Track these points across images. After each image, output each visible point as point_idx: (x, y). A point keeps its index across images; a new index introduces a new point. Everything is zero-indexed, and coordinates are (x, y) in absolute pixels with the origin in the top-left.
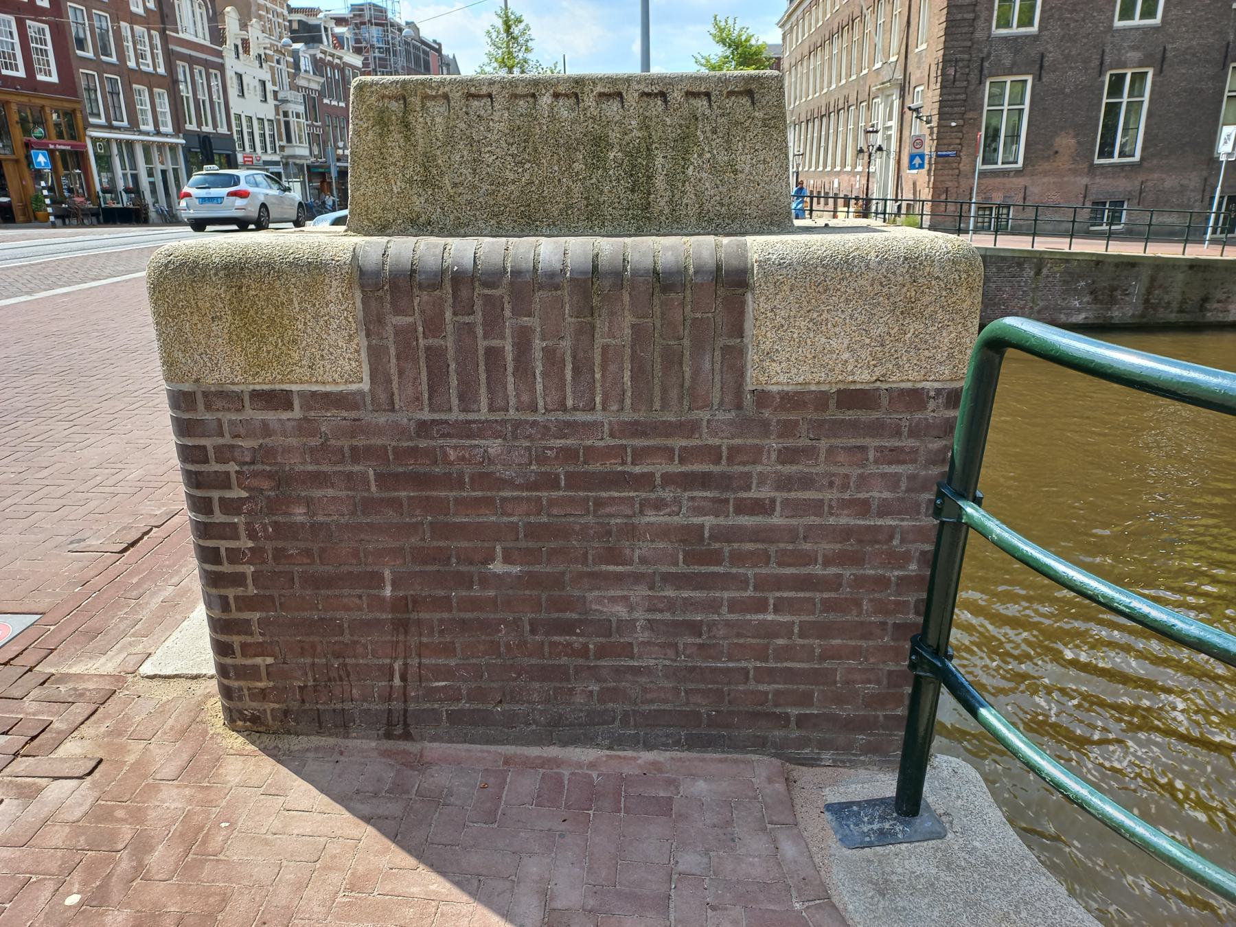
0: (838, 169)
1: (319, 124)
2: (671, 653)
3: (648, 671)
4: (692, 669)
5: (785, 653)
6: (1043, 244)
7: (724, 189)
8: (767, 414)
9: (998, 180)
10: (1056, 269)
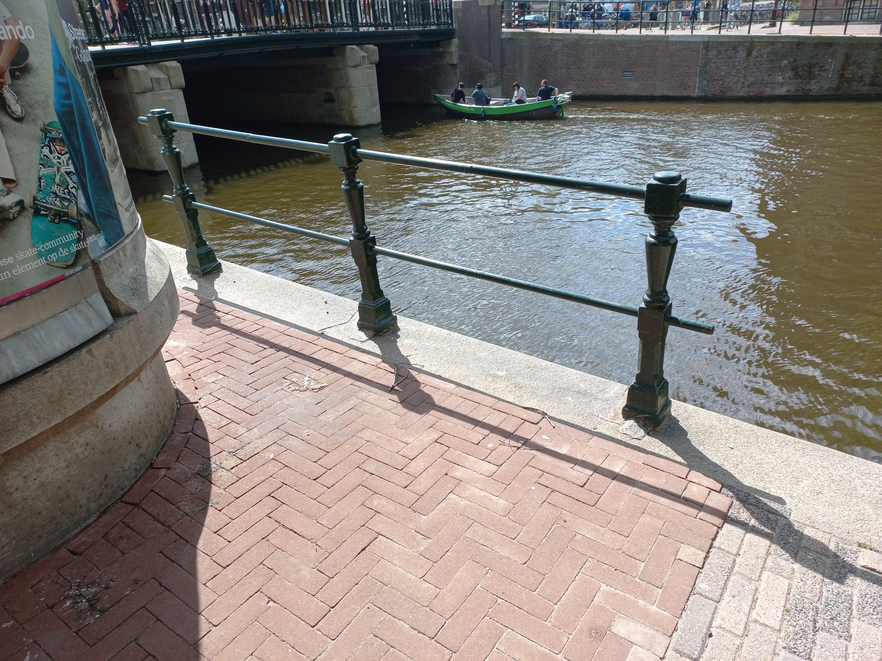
10: (763, 50)
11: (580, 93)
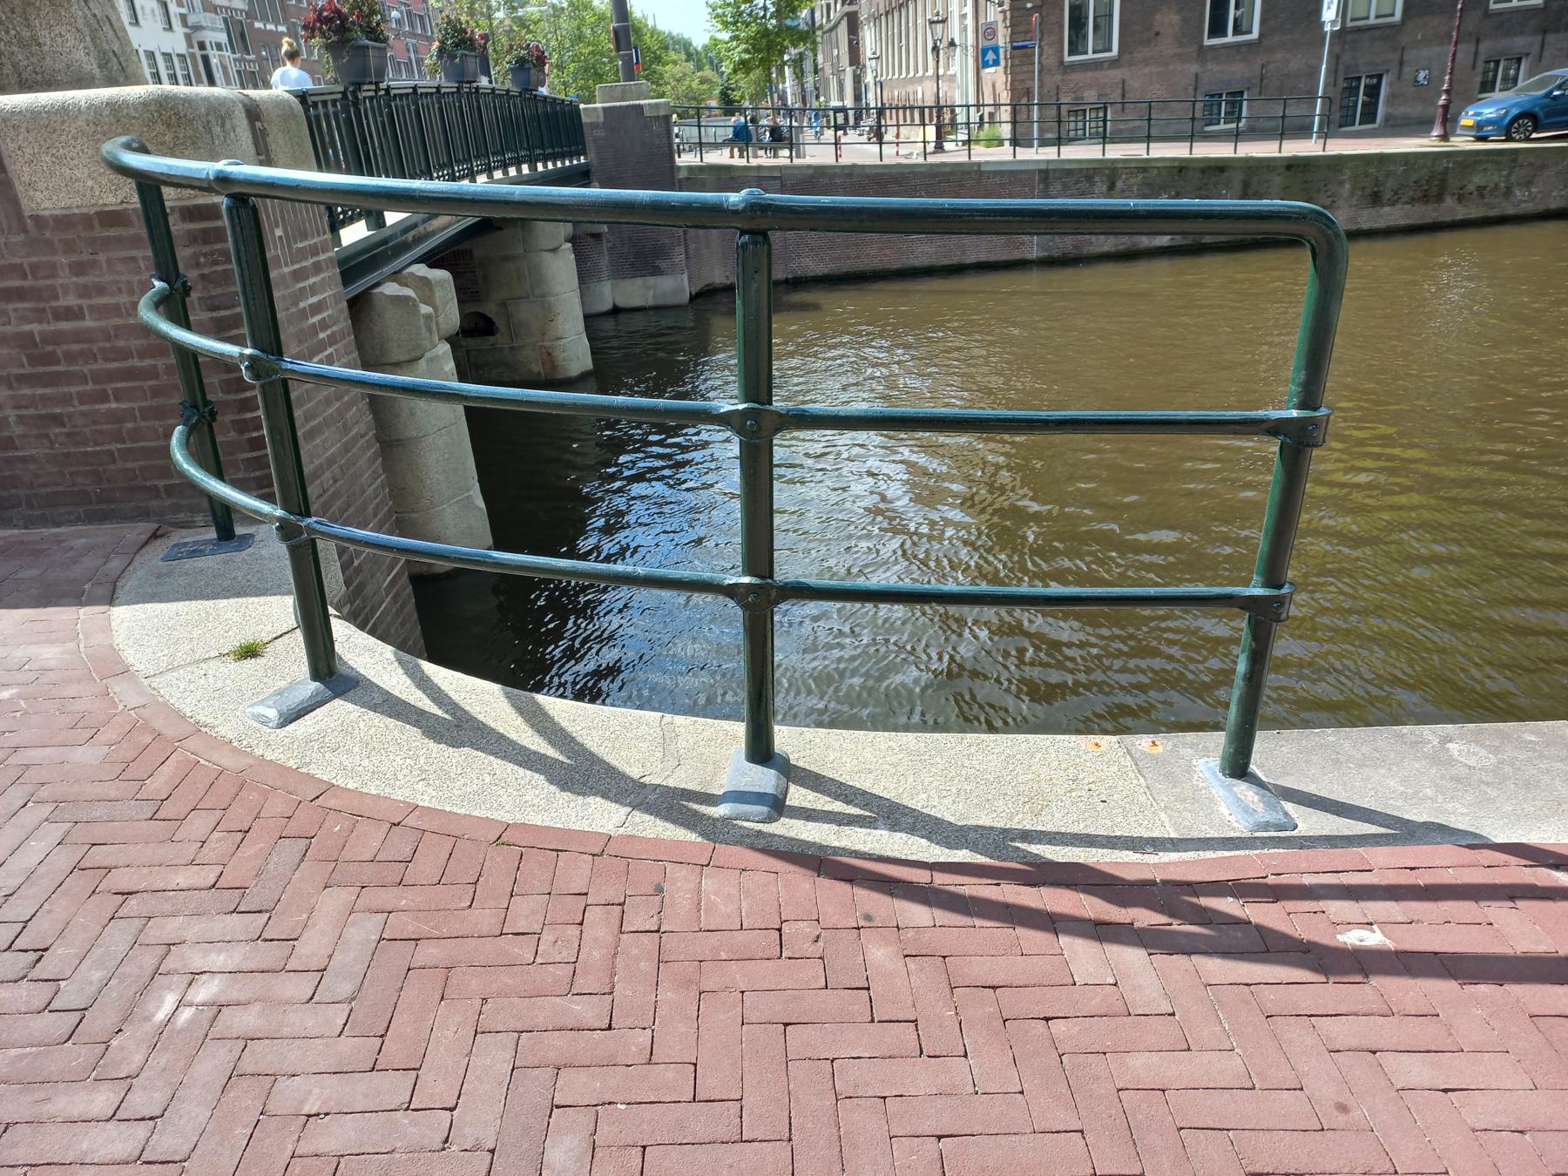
0: (920, 73)
1: (252, 57)
2: (45, 441)
3: (32, 459)
4: (67, 455)
5: (136, 435)
6: (1116, 152)
7: (34, 60)
8: (48, 234)
9: (1090, 74)
10: (1133, 181)
11: (826, 271)
